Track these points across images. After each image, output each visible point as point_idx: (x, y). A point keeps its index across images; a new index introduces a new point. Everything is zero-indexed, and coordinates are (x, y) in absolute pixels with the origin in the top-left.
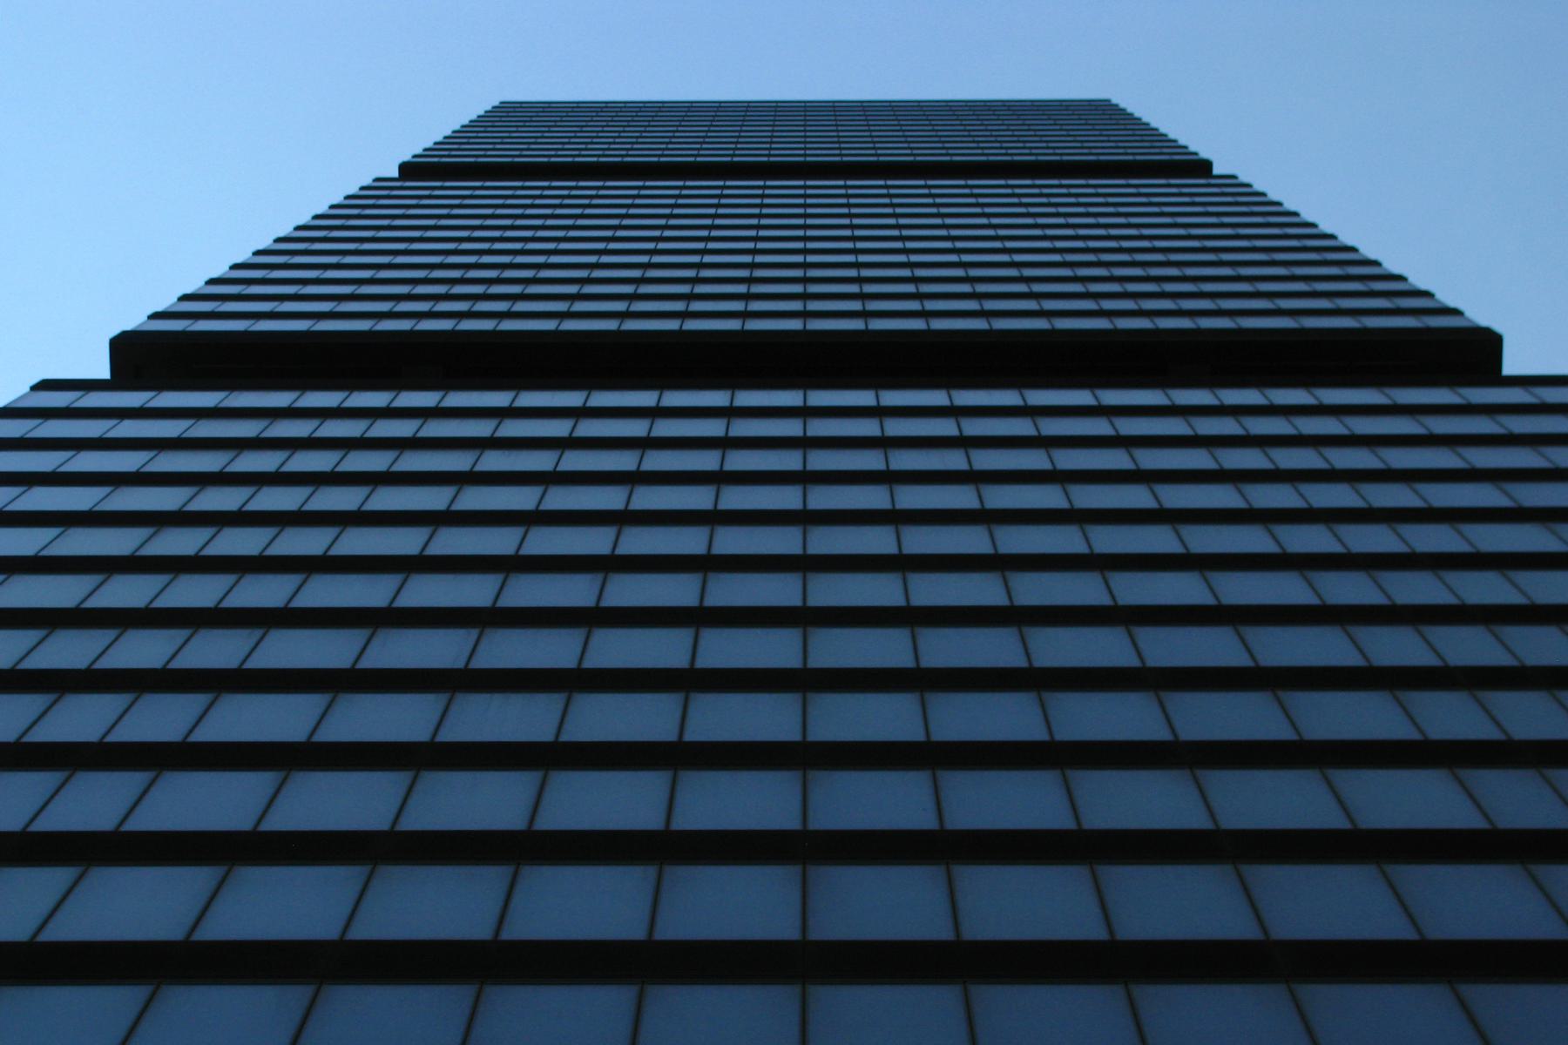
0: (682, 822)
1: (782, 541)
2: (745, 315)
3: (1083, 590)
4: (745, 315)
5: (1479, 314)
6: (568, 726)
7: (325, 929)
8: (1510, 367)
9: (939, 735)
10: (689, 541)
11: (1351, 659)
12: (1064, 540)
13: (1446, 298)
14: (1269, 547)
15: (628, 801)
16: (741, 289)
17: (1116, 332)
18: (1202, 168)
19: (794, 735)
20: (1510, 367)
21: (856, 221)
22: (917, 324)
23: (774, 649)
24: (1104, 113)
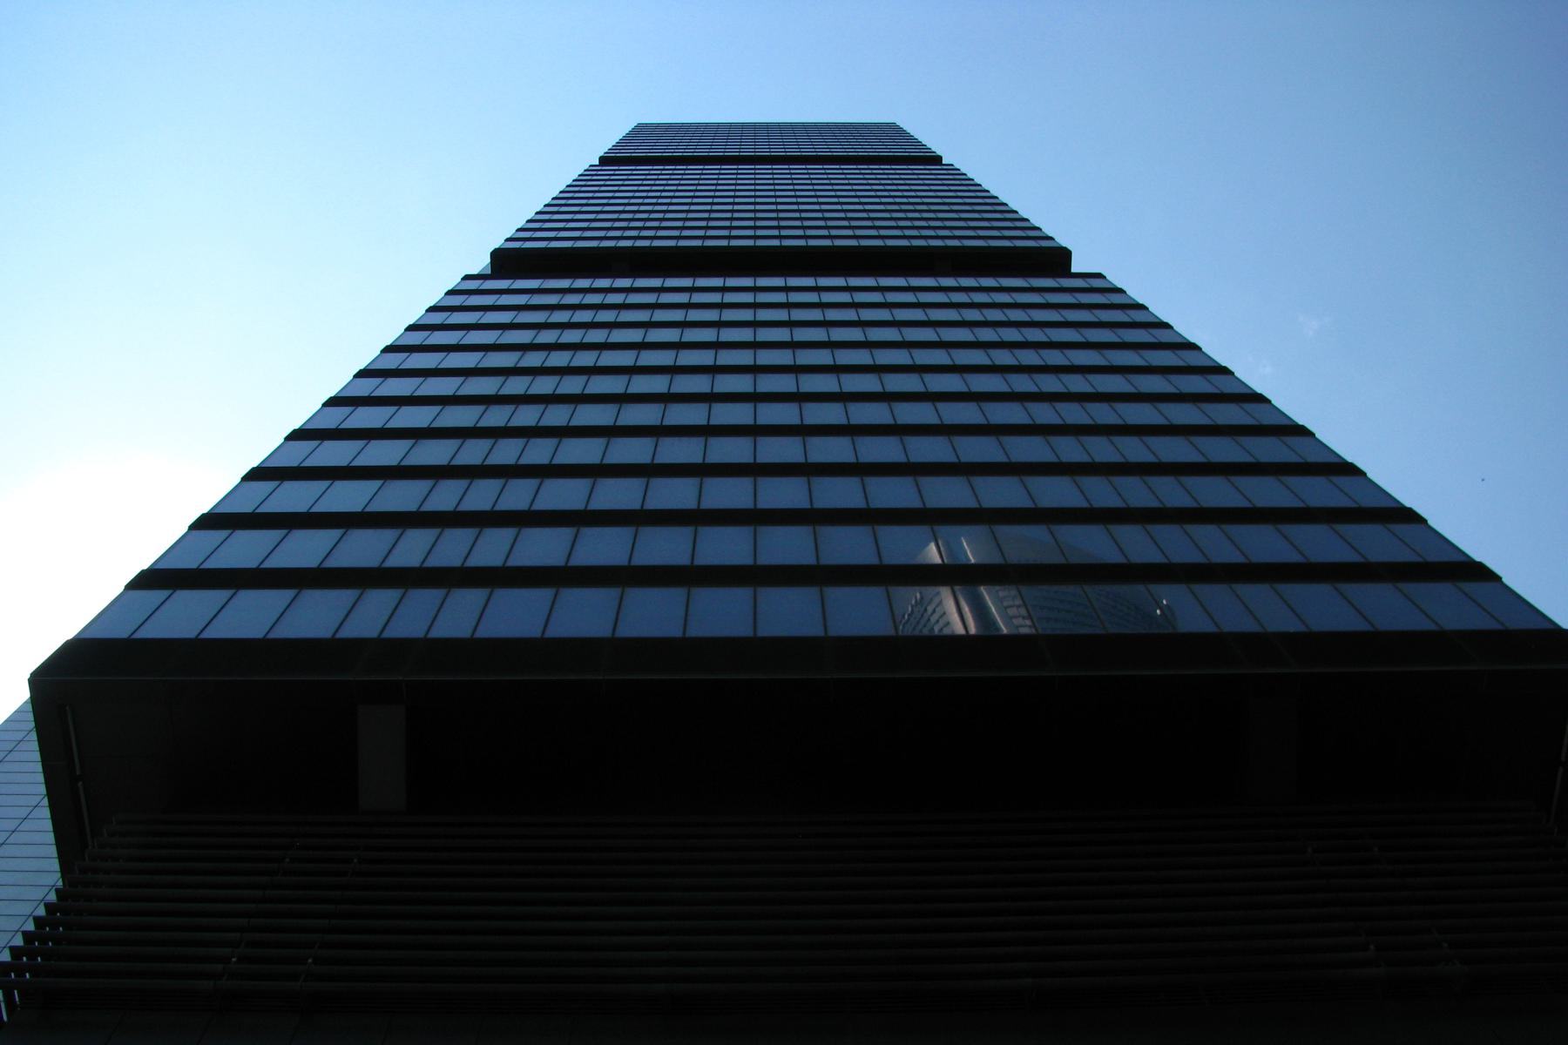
0: (706, 505)
1: (747, 315)
2: (729, 238)
3: (855, 334)
4: (729, 238)
5: (1062, 240)
6: (648, 500)
7: (578, 505)
8: (1074, 269)
9: (819, 505)
10: (712, 315)
11: (948, 362)
12: (850, 315)
13: (1048, 231)
14: (914, 300)
15: (699, 384)
16: (727, 224)
17: (886, 247)
18: (937, 160)
19: (751, 390)
20: (1074, 269)
21: (783, 223)
22: (802, 243)
23: (745, 335)
24: (893, 132)
